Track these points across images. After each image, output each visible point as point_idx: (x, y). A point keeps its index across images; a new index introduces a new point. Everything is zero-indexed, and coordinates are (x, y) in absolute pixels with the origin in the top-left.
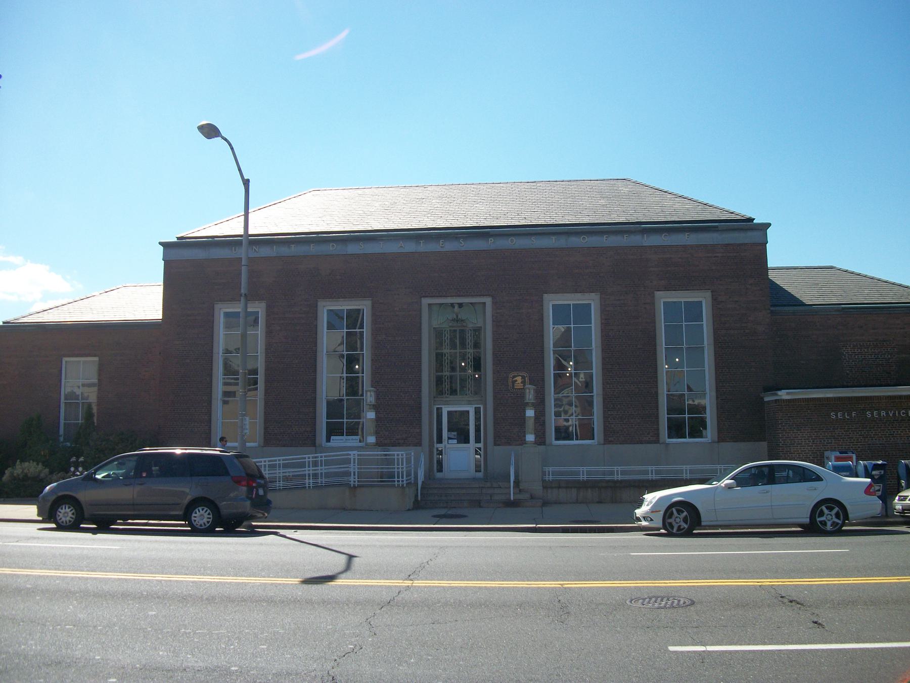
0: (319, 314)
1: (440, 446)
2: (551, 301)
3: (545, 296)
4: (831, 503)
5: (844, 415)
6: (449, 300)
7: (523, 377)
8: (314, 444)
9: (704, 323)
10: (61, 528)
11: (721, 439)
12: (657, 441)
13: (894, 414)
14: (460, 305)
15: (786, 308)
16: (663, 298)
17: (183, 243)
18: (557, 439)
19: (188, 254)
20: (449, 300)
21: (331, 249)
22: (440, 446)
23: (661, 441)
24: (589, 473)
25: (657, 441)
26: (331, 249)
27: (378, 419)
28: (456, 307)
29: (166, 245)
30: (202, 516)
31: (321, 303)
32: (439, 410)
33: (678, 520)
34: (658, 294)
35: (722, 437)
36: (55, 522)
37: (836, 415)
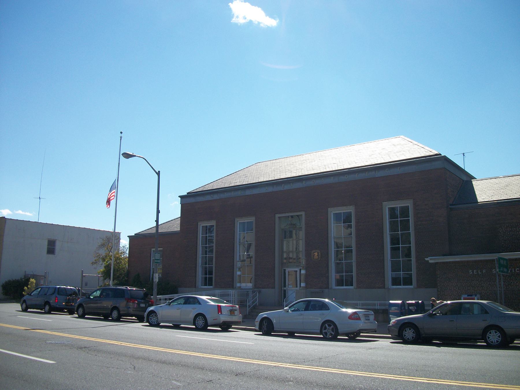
0: (236, 224)
1: (285, 288)
2: (332, 212)
3: (329, 209)
4: (329, 322)
5: (477, 272)
6: (287, 214)
7: (318, 253)
8: (195, 287)
9: (201, 236)
10: (406, 342)
11: (419, 286)
12: (384, 287)
13: (511, 271)
14: (292, 217)
15: (460, 206)
16: (387, 206)
17: (190, 195)
18: (393, 285)
19: (192, 200)
20: (287, 214)
21: (239, 193)
22: (285, 288)
23: (386, 287)
24: (380, 305)
25: (384, 287)
26: (239, 193)
27: (306, 275)
28: (290, 219)
29: (182, 197)
30: (494, 337)
31: (236, 220)
32: (285, 270)
33: (329, 330)
34: (384, 203)
35: (419, 286)
36: (486, 341)
37: (473, 272)
